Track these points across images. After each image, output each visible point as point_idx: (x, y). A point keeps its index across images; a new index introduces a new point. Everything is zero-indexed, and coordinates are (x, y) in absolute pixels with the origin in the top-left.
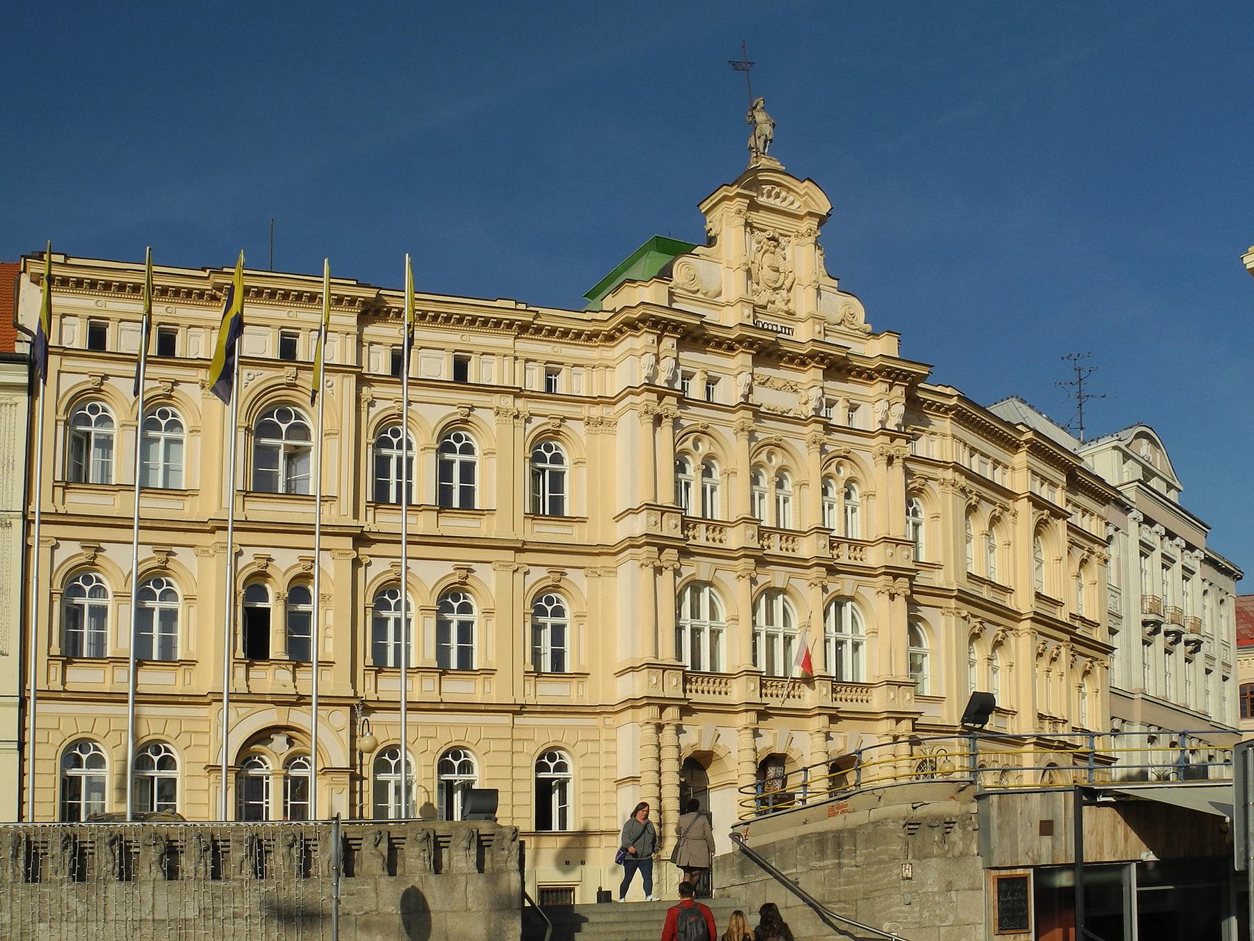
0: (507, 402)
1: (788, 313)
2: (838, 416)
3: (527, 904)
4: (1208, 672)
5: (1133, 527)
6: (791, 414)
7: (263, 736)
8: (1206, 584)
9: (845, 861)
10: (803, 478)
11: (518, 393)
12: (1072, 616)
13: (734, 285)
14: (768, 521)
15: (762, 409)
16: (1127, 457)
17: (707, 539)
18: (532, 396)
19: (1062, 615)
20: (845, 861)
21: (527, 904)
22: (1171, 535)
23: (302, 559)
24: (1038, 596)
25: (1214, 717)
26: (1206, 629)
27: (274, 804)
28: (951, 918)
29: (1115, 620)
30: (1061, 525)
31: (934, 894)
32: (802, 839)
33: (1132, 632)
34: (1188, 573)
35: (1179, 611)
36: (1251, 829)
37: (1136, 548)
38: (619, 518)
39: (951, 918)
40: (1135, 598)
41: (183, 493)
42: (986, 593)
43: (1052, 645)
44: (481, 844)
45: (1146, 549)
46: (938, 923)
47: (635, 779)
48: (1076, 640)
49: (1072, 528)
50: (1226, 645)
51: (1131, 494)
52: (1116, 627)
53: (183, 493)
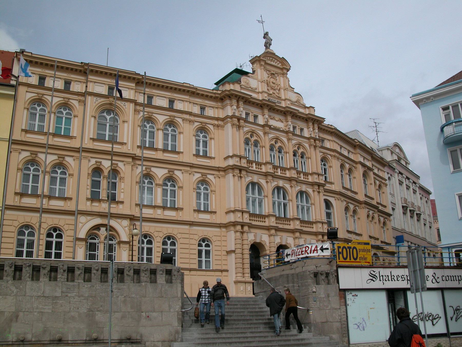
0: (187, 117)
1: (279, 97)
2: (298, 132)
3: (185, 296)
4: (425, 225)
5: (396, 175)
6: (281, 129)
7: (97, 227)
8: (421, 196)
9: (295, 285)
10: (126, 119)
11: (190, 114)
12: (378, 203)
13: (262, 87)
14: (277, 164)
15: (272, 127)
16: (392, 153)
17: (256, 168)
18: (195, 115)
19: (374, 203)
20: (295, 285)
21: (185, 296)
22: (408, 178)
23: (96, 162)
24: (366, 195)
25: (429, 240)
26: (422, 210)
27: (101, 253)
28: (330, 307)
29: (394, 205)
30: (371, 174)
31: (323, 298)
32: (281, 276)
33: (399, 210)
34: (415, 192)
35: (413, 204)
36: (361, 287)
37: (398, 182)
38: (226, 158)
39: (330, 307)
40: (399, 198)
41: (178, 153)
42: (349, 194)
43: (371, 212)
44: (169, 272)
45: (401, 183)
46: (325, 308)
47: (234, 251)
48: (380, 211)
49: (374, 174)
50: (429, 215)
51: (395, 165)
52: (394, 208)
53: (178, 153)
